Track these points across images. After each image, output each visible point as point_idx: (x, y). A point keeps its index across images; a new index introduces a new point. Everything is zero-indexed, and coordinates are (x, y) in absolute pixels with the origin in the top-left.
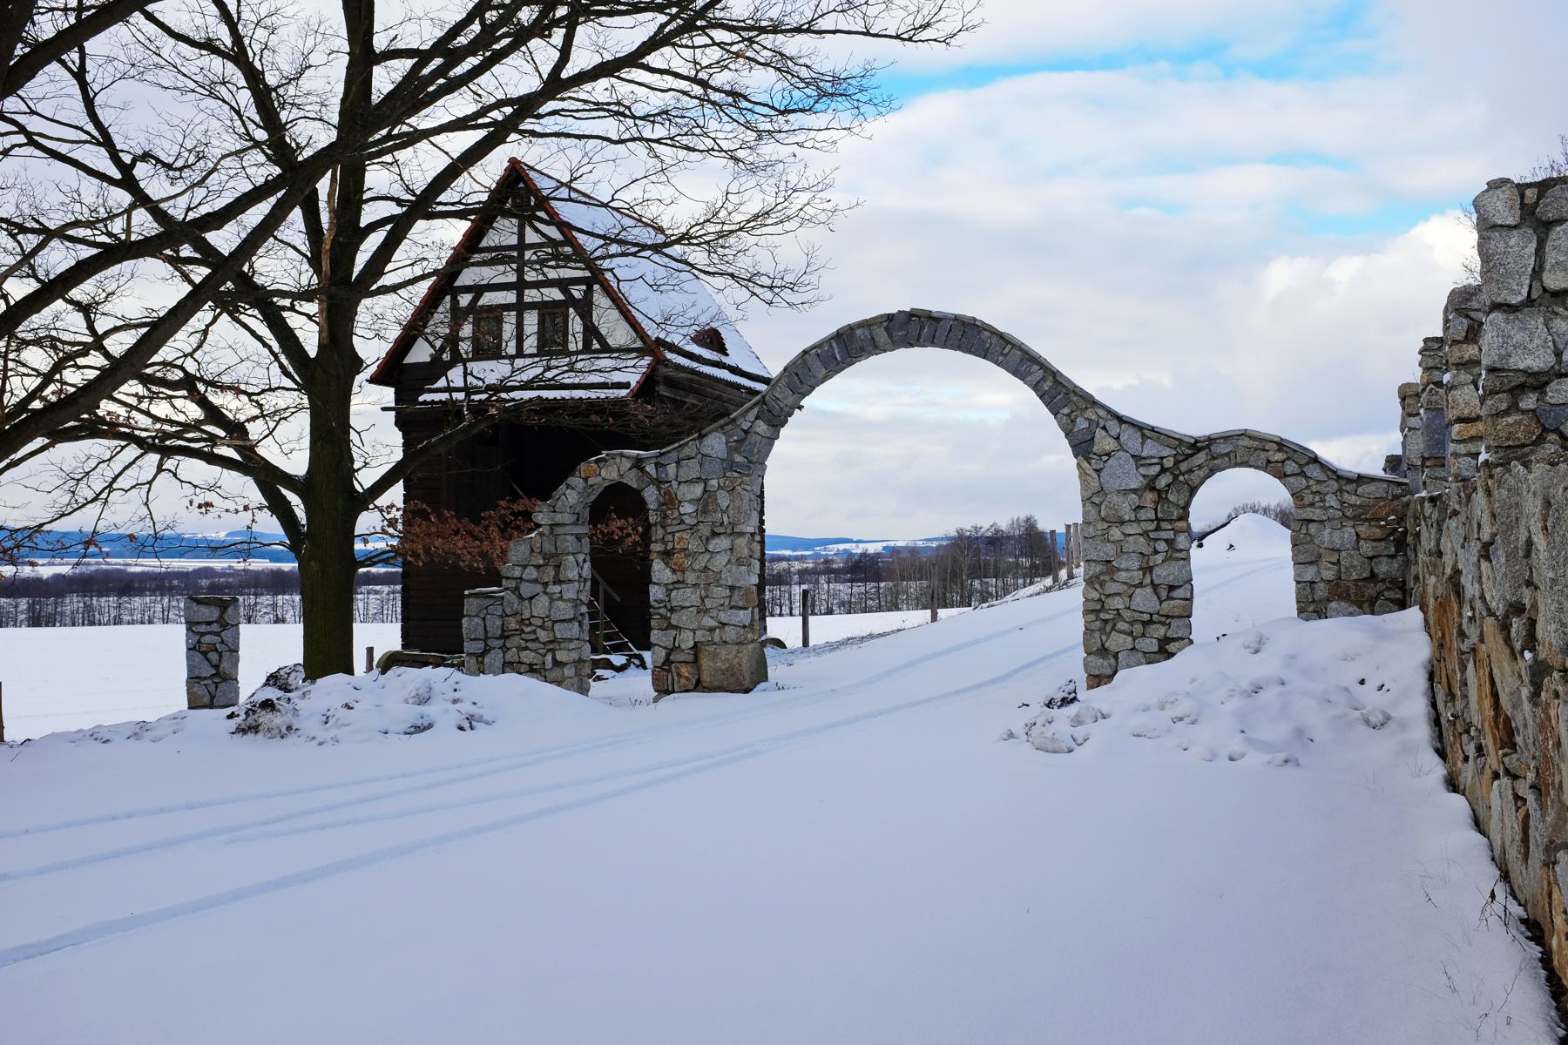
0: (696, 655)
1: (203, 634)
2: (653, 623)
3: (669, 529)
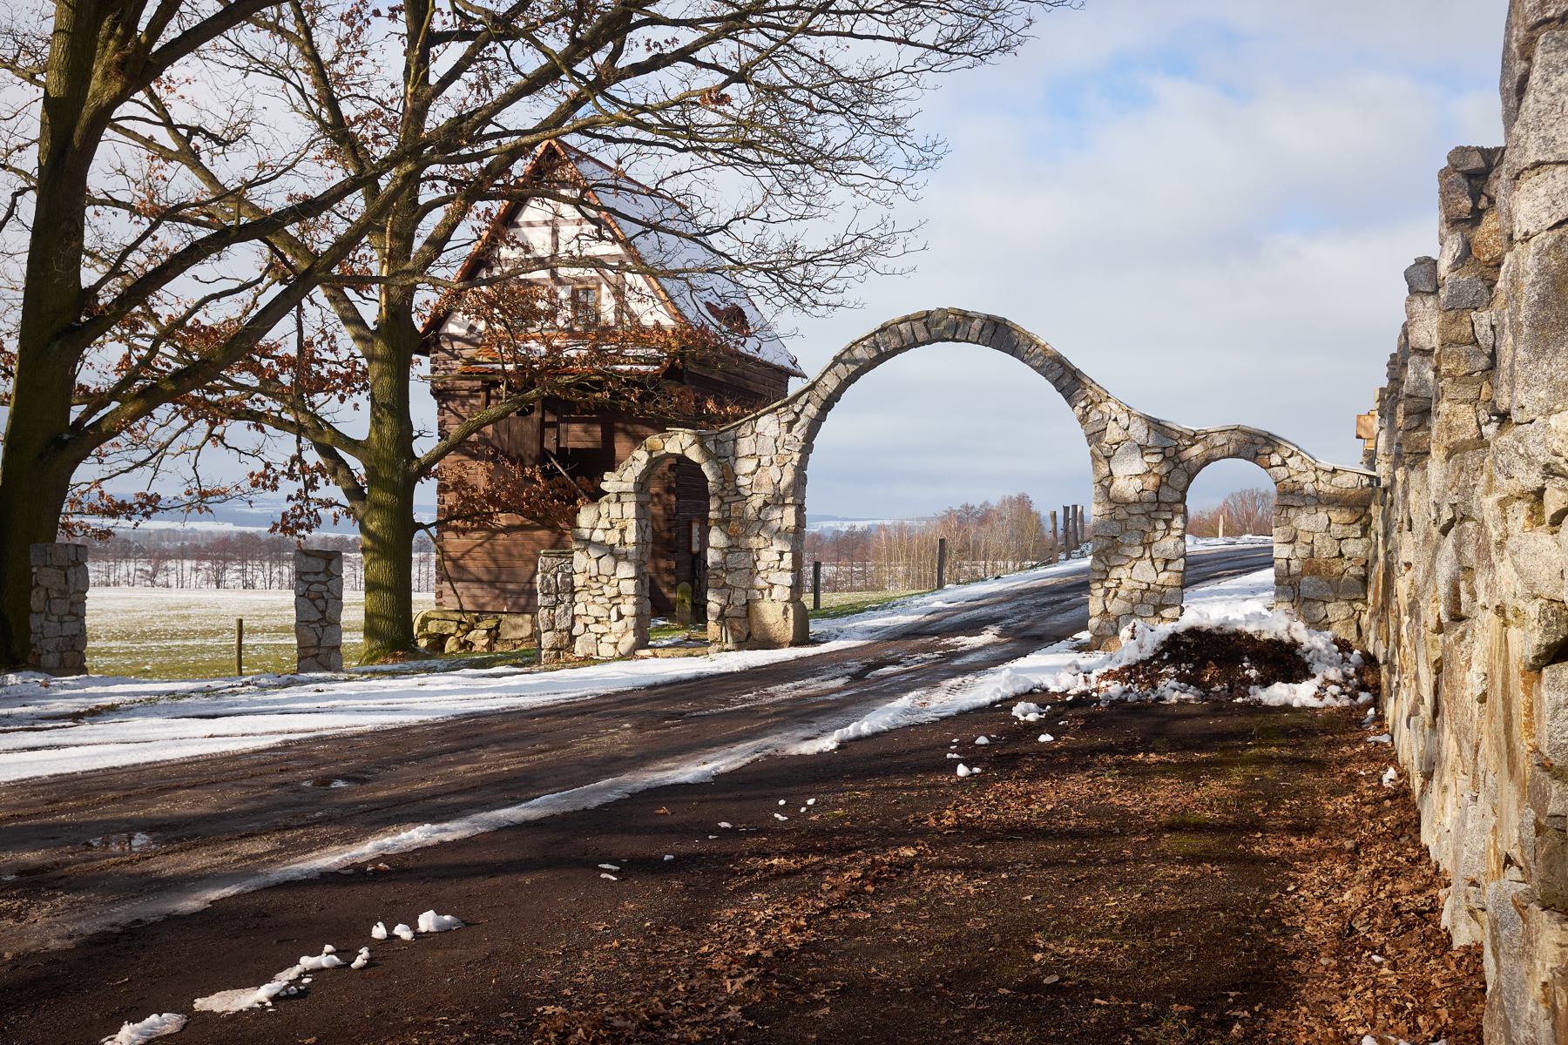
0: (747, 611)
1: (311, 583)
2: (710, 582)
3: (726, 500)
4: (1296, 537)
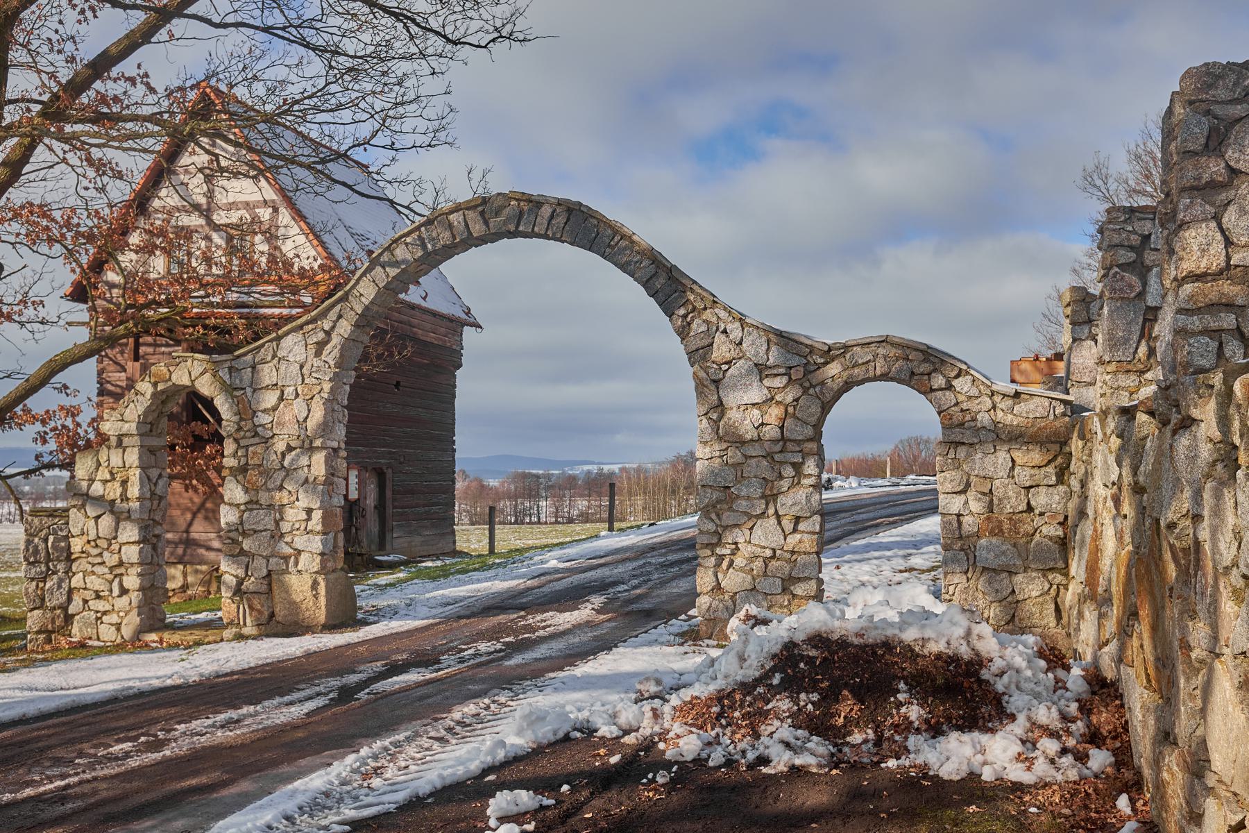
3: (243, 443)
4: (968, 485)
